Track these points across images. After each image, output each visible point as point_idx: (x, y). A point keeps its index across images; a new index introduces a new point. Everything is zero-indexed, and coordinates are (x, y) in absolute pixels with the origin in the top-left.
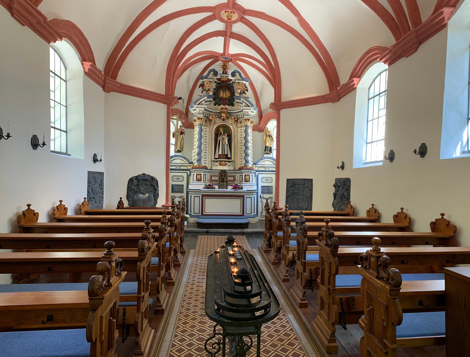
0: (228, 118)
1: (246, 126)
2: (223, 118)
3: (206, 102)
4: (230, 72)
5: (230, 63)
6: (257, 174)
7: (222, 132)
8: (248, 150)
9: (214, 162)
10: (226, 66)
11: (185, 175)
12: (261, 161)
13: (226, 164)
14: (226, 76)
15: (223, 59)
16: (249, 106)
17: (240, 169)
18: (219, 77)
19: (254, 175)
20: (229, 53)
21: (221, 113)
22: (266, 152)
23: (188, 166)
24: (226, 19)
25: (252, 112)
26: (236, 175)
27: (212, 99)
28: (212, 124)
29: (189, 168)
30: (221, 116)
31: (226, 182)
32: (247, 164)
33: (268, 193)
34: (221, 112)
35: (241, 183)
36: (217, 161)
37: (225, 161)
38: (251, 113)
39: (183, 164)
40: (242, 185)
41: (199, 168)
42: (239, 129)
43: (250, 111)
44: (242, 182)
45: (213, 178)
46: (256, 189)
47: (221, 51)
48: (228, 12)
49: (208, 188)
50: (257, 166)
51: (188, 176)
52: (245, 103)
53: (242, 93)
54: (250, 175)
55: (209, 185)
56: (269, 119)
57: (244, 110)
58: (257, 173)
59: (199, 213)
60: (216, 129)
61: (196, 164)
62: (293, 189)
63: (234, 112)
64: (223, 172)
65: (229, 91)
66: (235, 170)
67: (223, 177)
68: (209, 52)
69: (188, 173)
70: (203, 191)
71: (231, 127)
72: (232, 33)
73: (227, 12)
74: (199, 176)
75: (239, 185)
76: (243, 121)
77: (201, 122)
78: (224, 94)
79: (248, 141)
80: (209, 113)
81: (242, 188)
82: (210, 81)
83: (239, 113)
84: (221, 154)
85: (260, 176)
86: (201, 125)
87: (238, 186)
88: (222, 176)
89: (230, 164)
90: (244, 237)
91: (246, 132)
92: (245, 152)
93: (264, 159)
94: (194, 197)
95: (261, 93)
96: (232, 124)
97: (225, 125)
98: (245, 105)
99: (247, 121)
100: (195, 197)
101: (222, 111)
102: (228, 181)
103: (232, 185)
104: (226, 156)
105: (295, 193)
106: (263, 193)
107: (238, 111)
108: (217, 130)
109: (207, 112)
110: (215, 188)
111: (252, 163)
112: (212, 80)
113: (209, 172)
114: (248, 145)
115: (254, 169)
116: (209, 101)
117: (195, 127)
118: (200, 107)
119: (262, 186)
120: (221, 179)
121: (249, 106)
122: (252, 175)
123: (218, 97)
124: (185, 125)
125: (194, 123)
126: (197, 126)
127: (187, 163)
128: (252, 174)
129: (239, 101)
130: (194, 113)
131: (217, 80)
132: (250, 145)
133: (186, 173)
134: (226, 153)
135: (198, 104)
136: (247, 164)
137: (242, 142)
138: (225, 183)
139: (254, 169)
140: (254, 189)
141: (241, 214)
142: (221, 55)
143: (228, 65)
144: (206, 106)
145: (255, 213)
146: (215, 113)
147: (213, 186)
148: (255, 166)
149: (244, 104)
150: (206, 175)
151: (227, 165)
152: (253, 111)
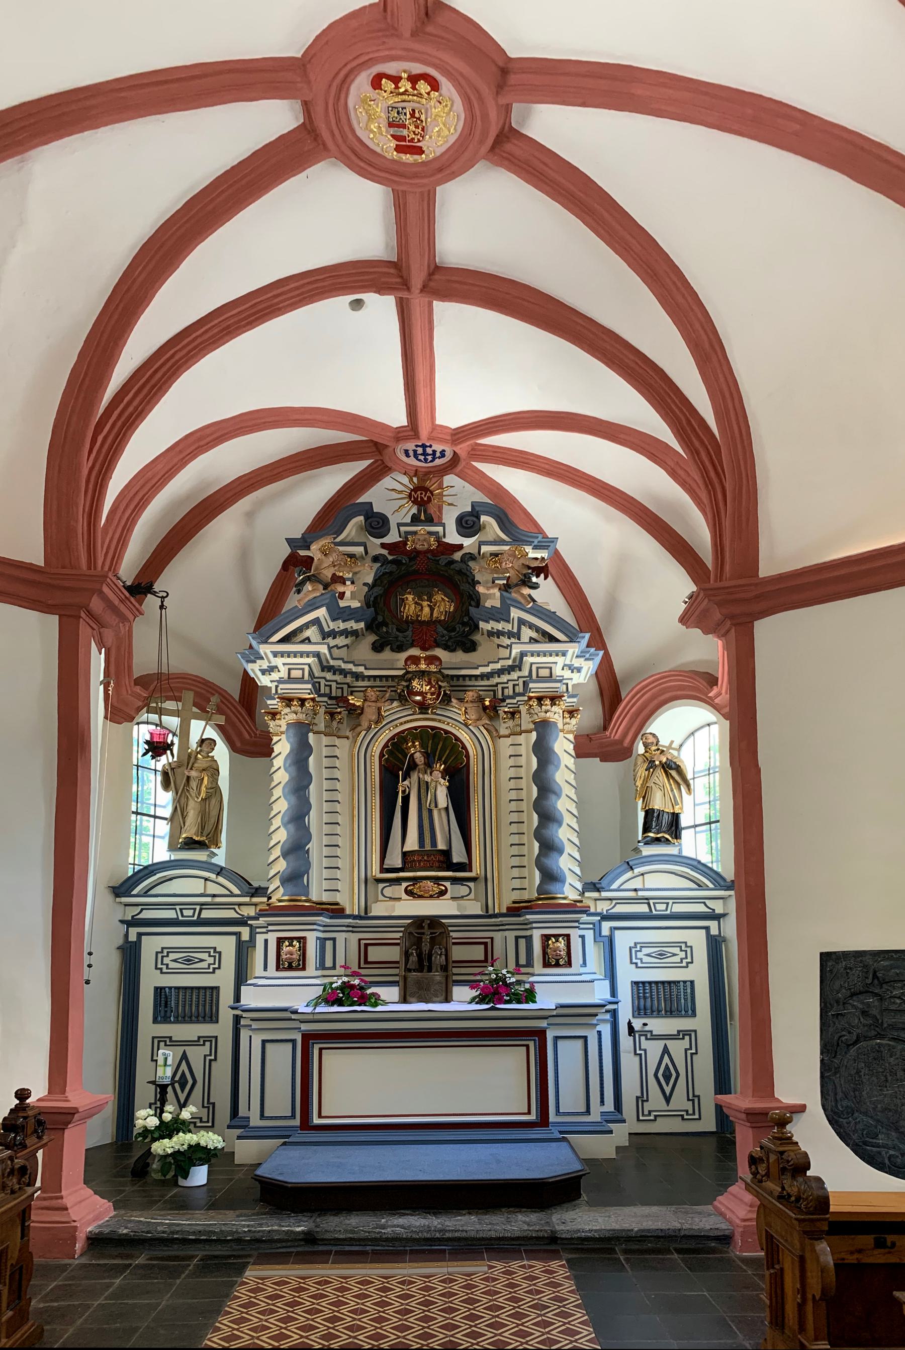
0: (446, 700)
1: (543, 727)
2: (418, 698)
3: (325, 635)
4: (450, 518)
5: (450, 479)
6: (605, 932)
7: (419, 758)
8: (555, 826)
9: (381, 886)
10: (426, 490)
11: (227, 946)
12: (629, 874)
13: (442, 893)
14: (430, 533)
15: (412, 461)
16: (552, 639)
17: (519, 909)
18: (393, 537)
19: (589, 935)
20: (438, 422)
21: (410, 681)
22: (651, 835)
23: (240, 905)
24: (385, 145)
25: (572, 668)
26: (498, 937)
27: (362, 625)
28: (365, 724)
29: (250, 911)
30: (412, 693)
31: (445, 968)
32: (553, 887)
33: (671, 1012)
34: (408, 672)
35: (523, 970)
36: (398, 881)
37: (436, 880)
38: (567, 674)
39: (214, 896)
40: (532, 983)
41: (293, 910)
42: (504, 743)
43: (560, 660)
44: (530, 963)
45: (375, 954)
46: (607, 996)
47: (398, 418)
48: (396, 80)
49: (341, 1004)
50: (604, 894)
51: (243, 951)
52: (531, 626)
53: (517, 585)
54: (575, 934)
55: (346, 986)
56: (656, 702)
57: (529, 659)
58: (606, 926)
59: (293, 1116)
60: (386, 746)
61: (279, 895)
62: (868, 1004)
63: (477, 672)
64: (425, 925)
65: (449, 591)
66: (490, 917)
67: (426, 948)
68: (325, 418)
69: (245, 936)
70: (311, 1017)
71: (464, 736)
72: (436, 270)
73: (389, 77)
74: (291, 945)
75: (513, 980)
76: (524, 709)
77: (302, 717)
78: (425, 603)
79: (556, 788)
80: (349, 679)
81: (530, 996)
82: (352, 556)
83: (504, 678)
84: (417, 848)
85: (624, 941)
86: (301, 730)
87: (507, 986)
88: (418, 942)
89: (463, 890)
90: (559, 1268)
91: (542, 750)
92: (538, 835)
93: (643, 864)
94: (264, 1042)
95: (613, 604)
96: (466, 725)
97: (433, 728)
98: (534, 635)
99: (548, 702)
100: (268, 1045)
101: (413, 668)
102: (450, 965)
103: (473, 985)
104: (444, 860)
105: (893, 1027)
106: (640, 1010)
107: (498, 666)
108: (390, 753)
109: (338, 678)
110: (376, 1000)
111: (579, 886)
112: (361, 549)
113: (353, 929)
114: (555, 808)
115: (592, 910)
116: (345, 633)
117: (275, 739)
118: (296, 654)
119: (636, 983)
120: (414, 958)
121: (557, 641)
122: (583, 937)
123: (396, 617)
124: (238, 744)
125: (272, 724)
126: (283, 737)
127: (236, 891)
128: (582, 932)
129: (500, 626)
130: (269, 684)
131: (385, 552)
132: (564, 805)
133: (234, 938)
134: (441, 846)
135: (283, 641)
136: (553, 887)
137: (523, 794)
138: (437, 976)
139: (592, 910)
140: (597, 1001)
141: (532, 1117)
142: (399, 435)
143: (441, 487)
144: (324, 649)
145: (609, 1106)
146: (378, 683)
147: (369, 992)
148: (595, 895)
149: (527, 633)
150: (334, 940)
151: (448, 896)
152: (577, 663)
